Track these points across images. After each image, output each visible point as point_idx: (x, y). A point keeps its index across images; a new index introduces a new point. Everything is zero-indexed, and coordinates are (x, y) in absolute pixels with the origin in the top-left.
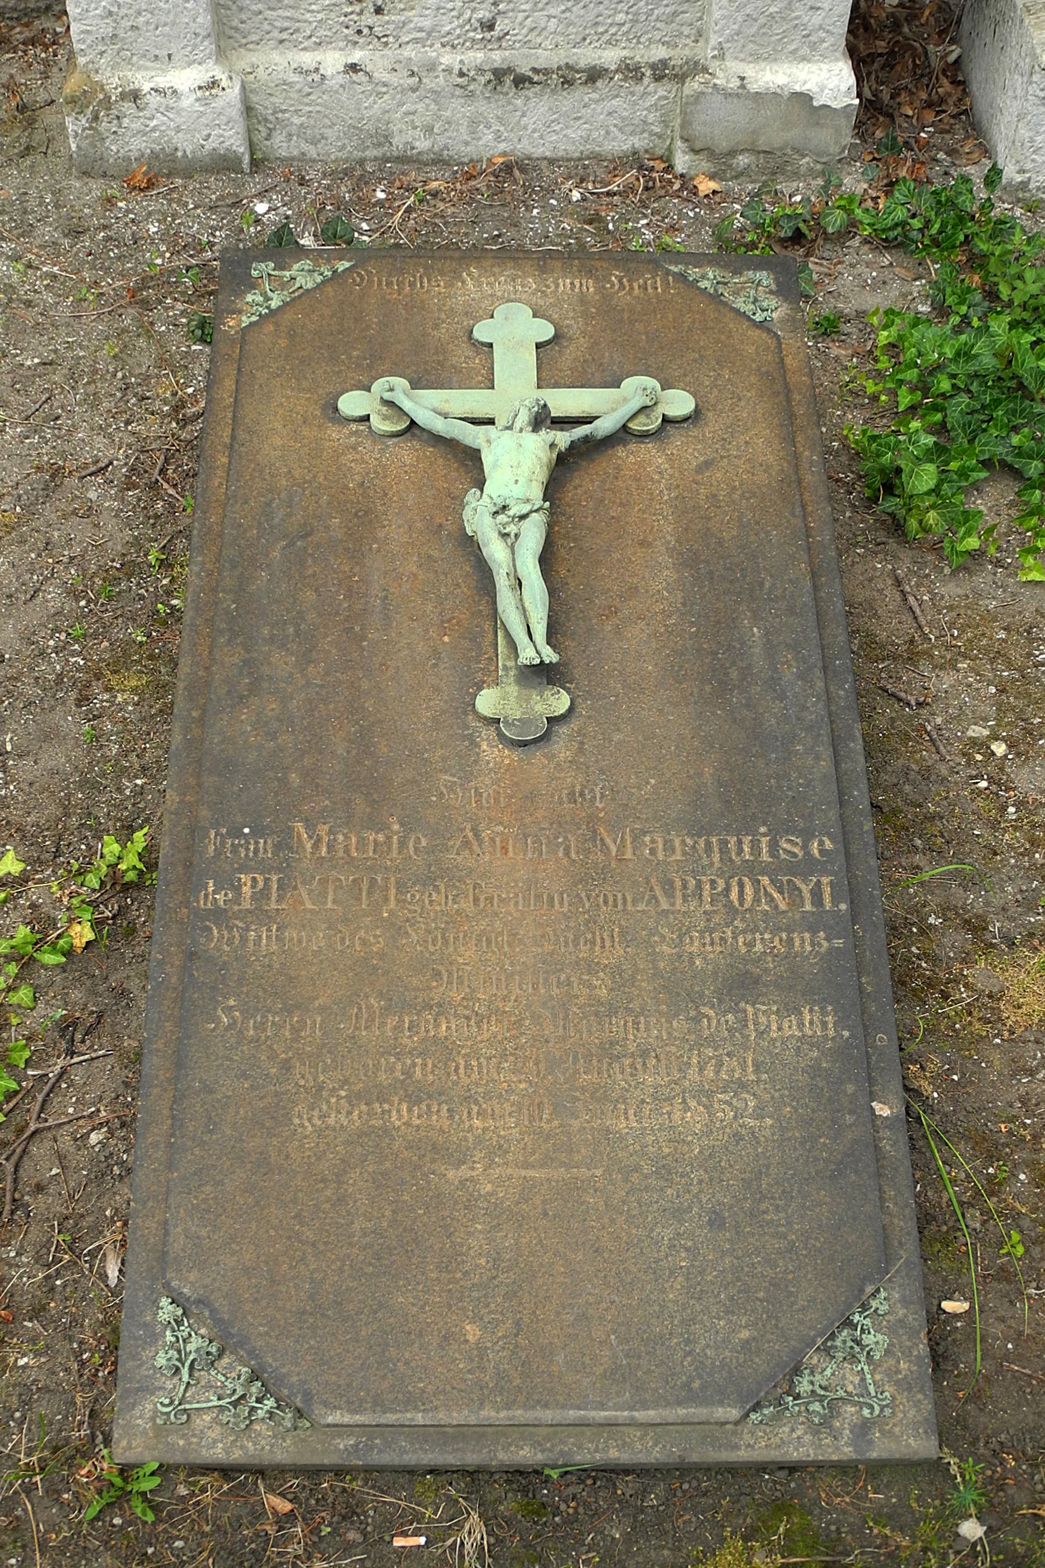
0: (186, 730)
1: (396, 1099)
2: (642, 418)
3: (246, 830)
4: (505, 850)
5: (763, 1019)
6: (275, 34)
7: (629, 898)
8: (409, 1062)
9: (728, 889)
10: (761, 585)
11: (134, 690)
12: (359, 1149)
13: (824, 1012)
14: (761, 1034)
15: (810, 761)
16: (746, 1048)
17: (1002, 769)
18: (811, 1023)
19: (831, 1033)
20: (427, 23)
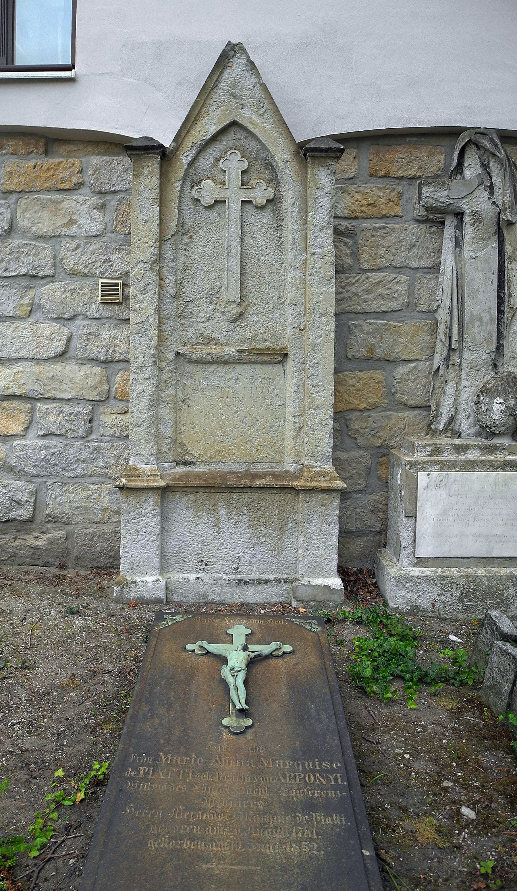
0: (128, 728)
1: (186, 839)
2: (276, 652)
3: (144, 755)
4: (229, 763)
5: (319, 818)
6: (177, 569)
7: (271, 779)
8: (192, 827)
9: (305, 777)
10: (314, 694)
11: (111, 729)
12: (171, 856)
13: (341, 816)
14: (318, 823)
15: (331, 741)
16: (313, 827)
17: (408, 762)
18: (336, 819)
19: (344, 823)
20: (219, 568)
